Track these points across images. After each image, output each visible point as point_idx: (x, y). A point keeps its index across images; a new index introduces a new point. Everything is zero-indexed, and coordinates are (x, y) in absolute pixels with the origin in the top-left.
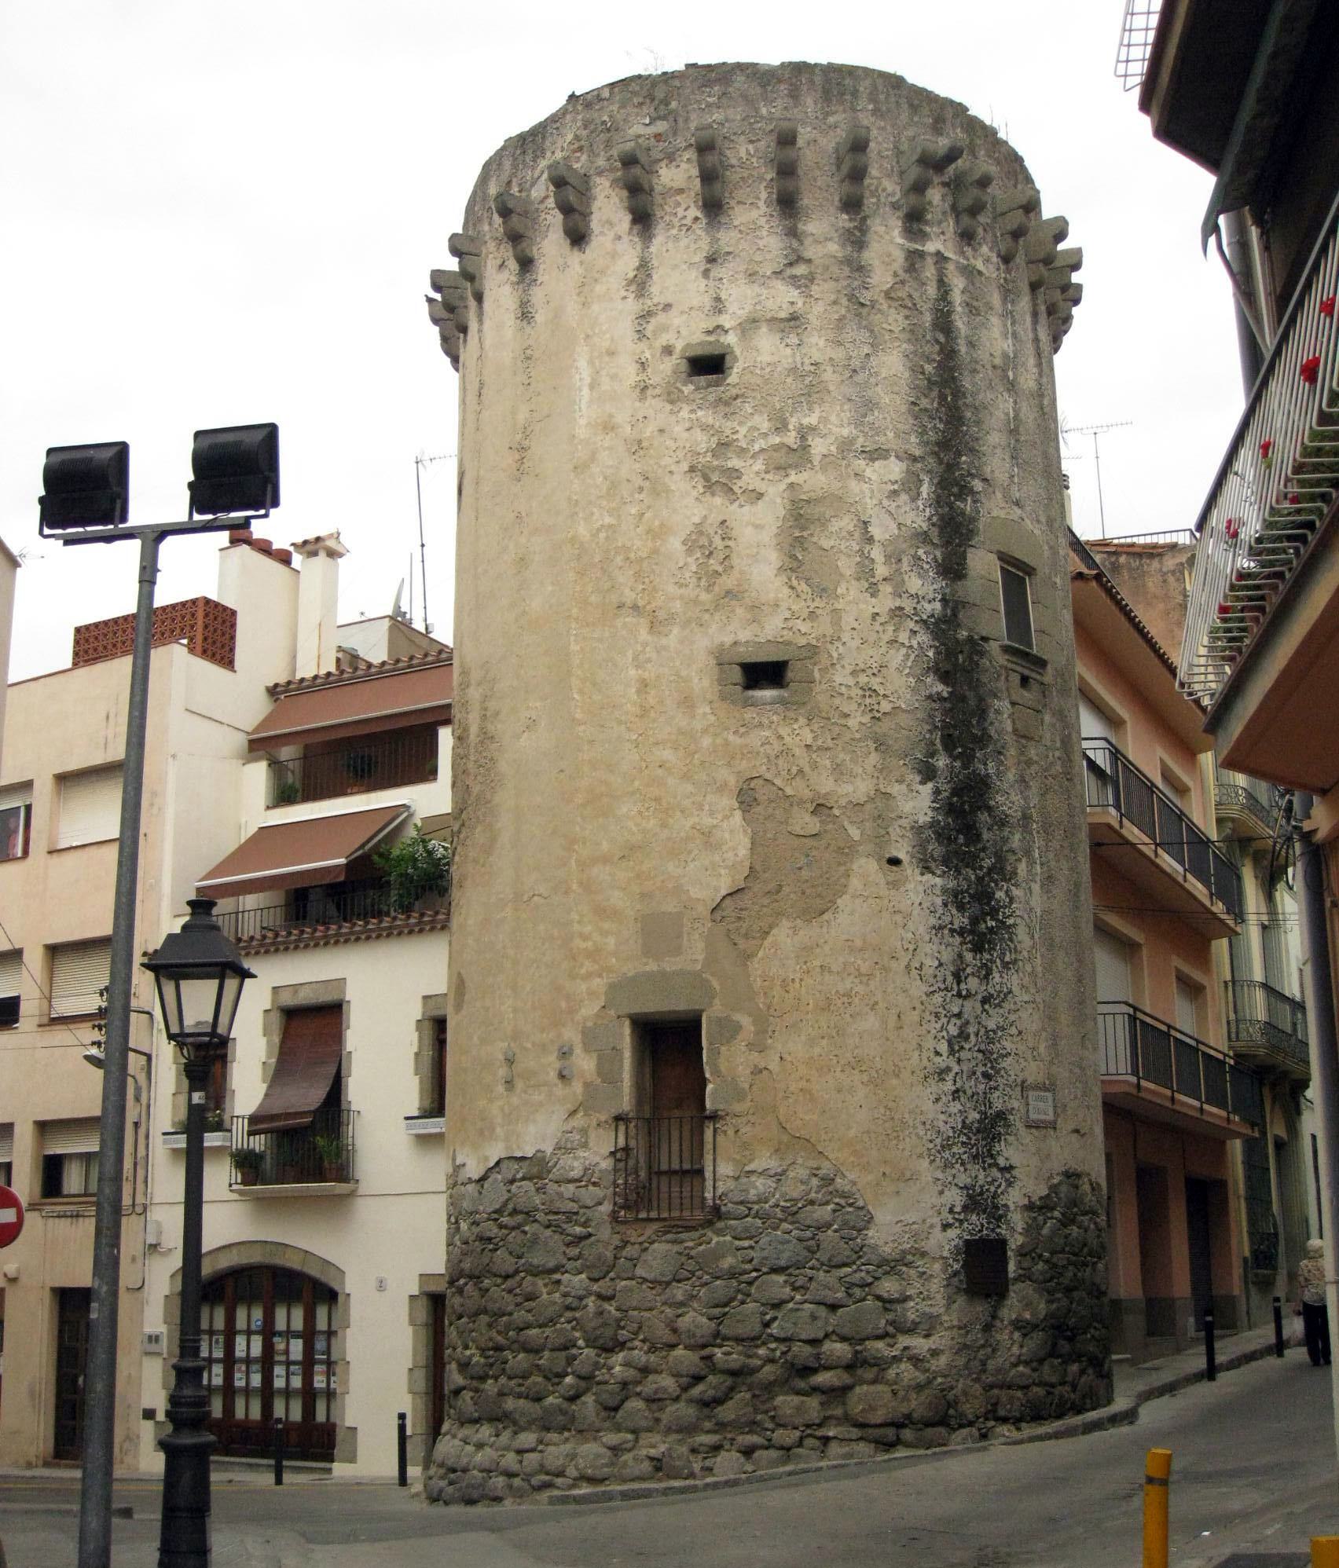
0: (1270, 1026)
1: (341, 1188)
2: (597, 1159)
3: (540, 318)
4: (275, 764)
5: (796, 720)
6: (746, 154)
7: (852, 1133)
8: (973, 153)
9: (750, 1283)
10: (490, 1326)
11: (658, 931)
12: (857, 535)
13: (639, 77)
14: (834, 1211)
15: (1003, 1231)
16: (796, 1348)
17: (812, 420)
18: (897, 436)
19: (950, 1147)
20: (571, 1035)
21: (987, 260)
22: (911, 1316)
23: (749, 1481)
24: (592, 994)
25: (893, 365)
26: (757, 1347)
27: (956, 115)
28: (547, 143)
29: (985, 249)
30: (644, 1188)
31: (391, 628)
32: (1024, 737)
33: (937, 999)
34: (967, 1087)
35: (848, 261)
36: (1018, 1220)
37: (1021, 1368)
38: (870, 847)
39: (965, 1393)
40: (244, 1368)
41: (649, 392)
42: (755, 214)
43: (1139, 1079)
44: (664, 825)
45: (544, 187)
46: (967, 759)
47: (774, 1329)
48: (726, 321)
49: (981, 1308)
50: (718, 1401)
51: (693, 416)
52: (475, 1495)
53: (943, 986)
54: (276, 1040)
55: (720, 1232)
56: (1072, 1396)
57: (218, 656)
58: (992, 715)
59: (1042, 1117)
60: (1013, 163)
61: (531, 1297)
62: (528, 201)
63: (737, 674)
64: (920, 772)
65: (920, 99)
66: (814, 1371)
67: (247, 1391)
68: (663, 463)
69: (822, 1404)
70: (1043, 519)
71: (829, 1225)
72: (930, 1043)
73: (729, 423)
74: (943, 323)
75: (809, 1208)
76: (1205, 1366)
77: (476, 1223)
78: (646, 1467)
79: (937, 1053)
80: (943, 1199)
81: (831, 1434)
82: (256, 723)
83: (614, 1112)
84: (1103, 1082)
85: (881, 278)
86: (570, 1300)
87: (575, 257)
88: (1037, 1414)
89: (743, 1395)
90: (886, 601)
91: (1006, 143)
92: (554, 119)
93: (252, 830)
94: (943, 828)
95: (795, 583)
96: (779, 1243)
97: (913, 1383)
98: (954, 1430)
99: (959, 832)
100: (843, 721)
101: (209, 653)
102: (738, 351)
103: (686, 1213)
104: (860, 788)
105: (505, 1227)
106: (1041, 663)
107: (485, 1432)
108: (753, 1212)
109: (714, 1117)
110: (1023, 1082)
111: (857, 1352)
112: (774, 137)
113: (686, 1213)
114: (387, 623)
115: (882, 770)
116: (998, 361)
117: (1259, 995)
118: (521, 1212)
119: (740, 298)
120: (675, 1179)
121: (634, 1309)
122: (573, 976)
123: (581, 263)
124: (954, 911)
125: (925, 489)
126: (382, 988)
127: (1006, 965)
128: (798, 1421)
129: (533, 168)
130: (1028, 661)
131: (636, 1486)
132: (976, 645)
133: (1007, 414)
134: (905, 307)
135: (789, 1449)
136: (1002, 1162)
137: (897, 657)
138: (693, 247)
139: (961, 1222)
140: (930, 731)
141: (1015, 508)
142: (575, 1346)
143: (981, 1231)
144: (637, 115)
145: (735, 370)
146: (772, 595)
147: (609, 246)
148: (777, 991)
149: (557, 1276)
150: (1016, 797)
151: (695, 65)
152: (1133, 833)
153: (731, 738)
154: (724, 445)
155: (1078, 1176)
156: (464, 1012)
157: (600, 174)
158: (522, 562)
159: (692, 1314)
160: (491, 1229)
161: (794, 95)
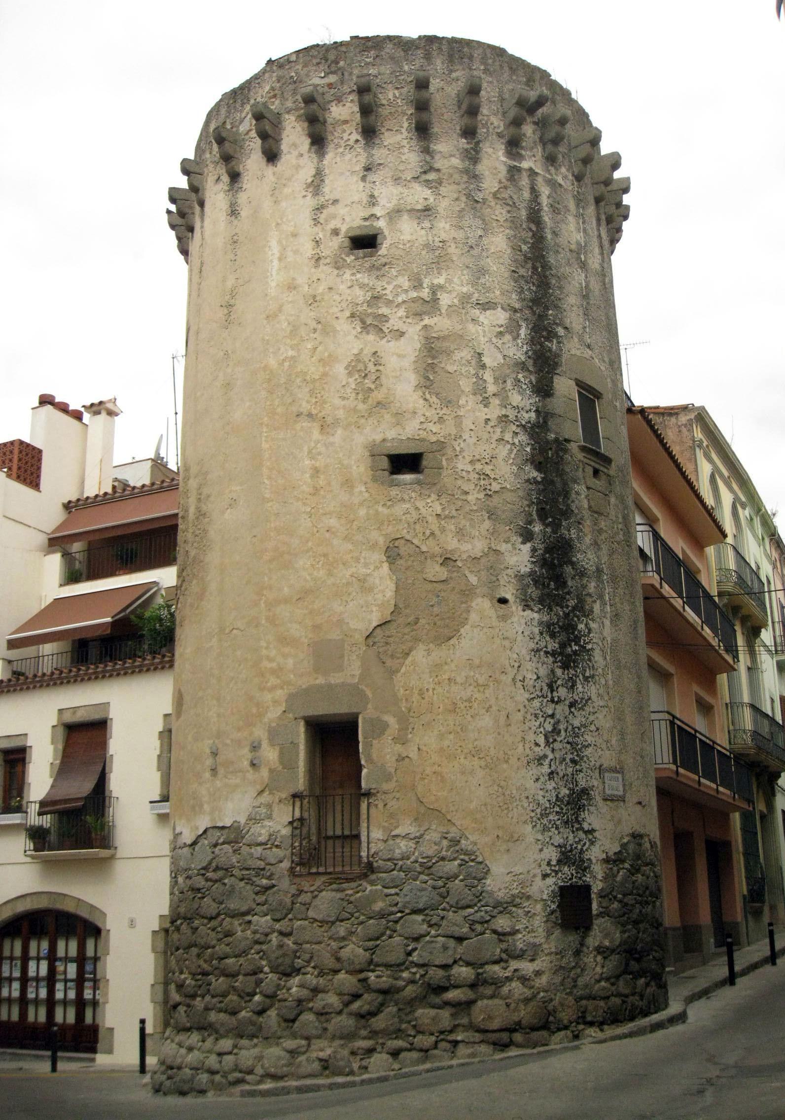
0: (755, 734)
1: (104, 853)
2: (279, 827)
3: (243, 214)
4: (66, 555)
5: (429, 496)
6: (394, 97)
7: (472, 806)
8: (554, 103)
9: (396, 922)
10: (198, 956)
11: (325, 654)
12: (473, 362)
13: (318, 45)
14: (460, 865)
15: (588, 879)
16: (432, 971)
17: (441, 280)
18: (502, 294)
19: (547, 815)
20: (260, 733)
21: (565, 177)
22: (520, 945)
23: (396, 1077)
24: (275, 702)
25: (499, 244)
26: (402, 971)
27: (542, 78)
28: (252, 93)
29: (563, 170)
30: (315, 849)
31: (152, 466)
32: (596, 512)
33: (536, 703)
34: (559, 770)
35: (466, 171)
36: (598, 870)
37: (603, 983)
38: (485, 590)
39: (562, 1005)
40: (34, 984)
41: (322, 262)
42: (399, 137)
43: (677, 767)
44: (330, 574)
45: (248, 124)
46: (556, 526)
47: (415, 957)
48: (378, 211)
49: (573, 938)
50: (372, 1014)
51: (353, 278)
52: (186, 1088)
53: (540, 694)
54: (60, 747)
55: (372, 883)
56: (641, 1003)
57: (28, 481)
58: (574, 496)
59: (616, 793)
60: (582, 116)
61: (228, 934)
62: (237, 133)
63: (385, 463)
64: (521, 535)
65: (517, 65)
66: (445, 989)
67: (36, 1002)
68: (331, 311)
69: (452, 1015)
70: (606, 359)
71: (456, 877)
72: (531, 737)
73: (380, 283)
74: (535, 217)
75: (441, 863)
76: (727, 974)
77: (189, 877)
78: (316, 1066)
79: (537, 745)
80: (543, 856)
81: (459, 1038)
82: (54, 527)
83: (292, 791)
84: (656, 769)
85: (490, 184)
86: (258, 936)
87: (270, 170)
88: (615, 1019)
89: (392, 1009)
90: (495, 411)
91: (577, 102)
92: (256, 77)
93: (49, 600)
94: (539, 577)
95: (428, 396)
96: (418, 891)
97: (522, 997)
98: (554, 1033)
99: (550, 579)
100: (464, 497)
101: (22, 478)
102: (386, 232)
103: (347, 868)
104: (477, 547)
105: (211, 880)
106: (607, 461)
107: (194, 1038)
108: (398, 867)
109: (368, 794)
110: (601, 766)
111: (478, 974)
112: (413, 86)
113: (347, 868)
114: (150, 463)
115: (494, 532)
116: (573, 247)
117: (747, 713)
118: (222, 869)
119: (389, 196)
120: (338, 843)
121: (307, 943)
122: (262, 689)
123: (274, 174)
124: (548, 638)
125: (523, 332)
126: (135, 709)
127: (586, 679)
128: (434, 1029)
129: (241, 112)
130: (600, 460)
131: (308, 1082)
132: (561, 444)
133: (581, 284)
134: (508, 205)
135: (427, 1051)
136: (586, 826)
137: (503, 451)
138: (354, 160)
139: (556, 872)
140: (529, 506)
141: (588, 350)
142: (261, 972)
143: (570, 879)
144: (316, 71)
145: (384, 245)
146: (411, 405)
147: (294, 161)
148: (416, 698)
149: (249, 918)
150: (591, 555)
151: (357, 37)
152: (667, 590)
153: (380, 509)
154: (376, 298)
155: (641, 836)
156: (182, 718)
157: (288, 113)
158: (228, 386)
159: (352, 946)
160: (200, 882)
161: (428, 57)
